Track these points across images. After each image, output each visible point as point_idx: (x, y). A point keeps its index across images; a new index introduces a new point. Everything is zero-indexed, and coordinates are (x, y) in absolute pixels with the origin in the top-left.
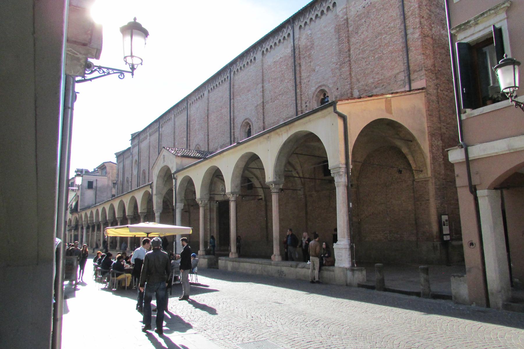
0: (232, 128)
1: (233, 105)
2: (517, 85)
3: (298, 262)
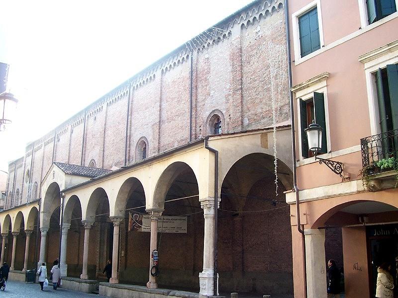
0: (128, 146)
1: (131, 121)
2: (320, 147)
3: (169, 290)
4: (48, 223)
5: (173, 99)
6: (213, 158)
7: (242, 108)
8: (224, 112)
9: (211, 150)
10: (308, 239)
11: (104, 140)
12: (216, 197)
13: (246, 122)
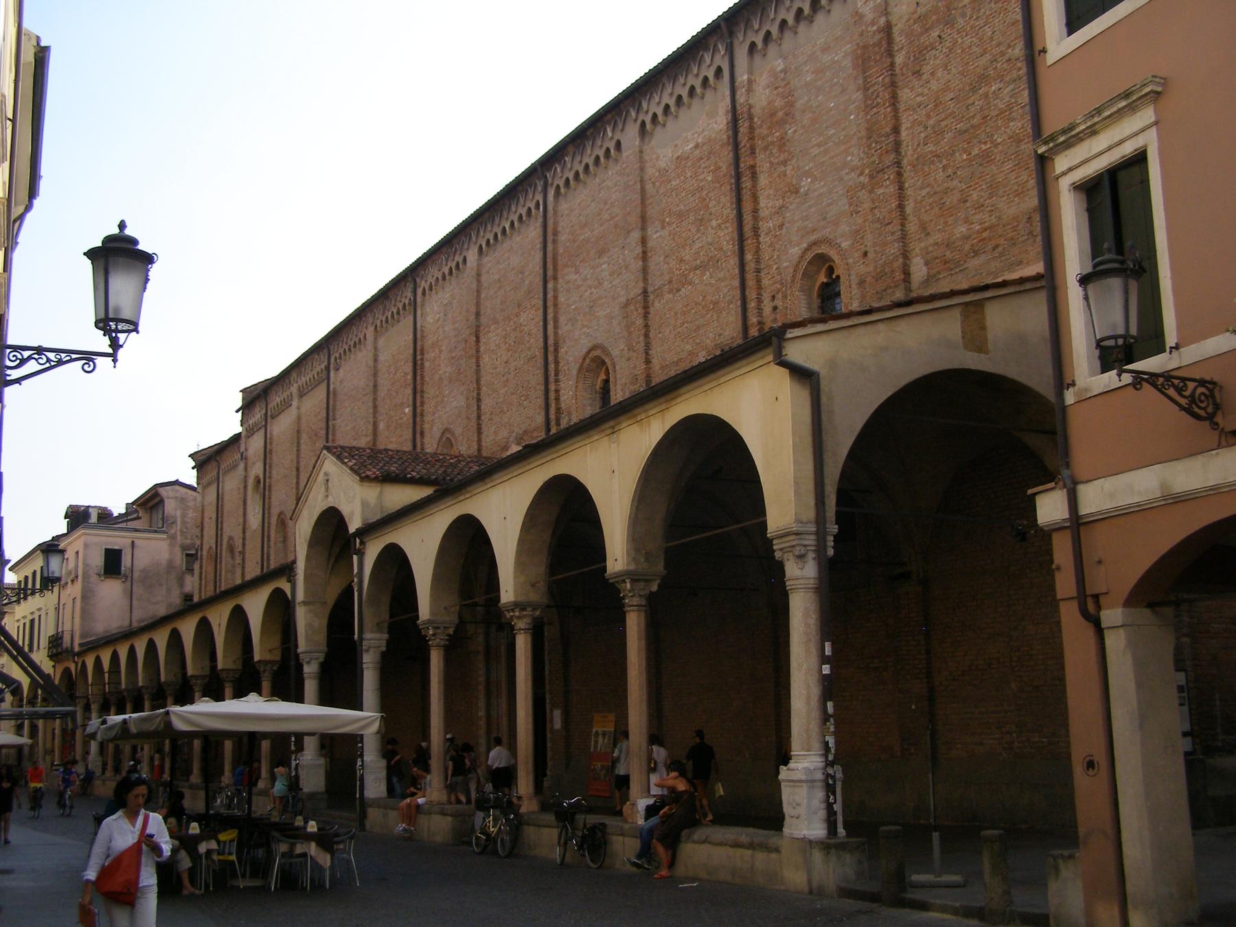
0: (552, 379)
1: (556, 298)
4: (322, 638)
5: (681, 216)
6: (804, 395)
7: (903, 225)
8: (845, 245)
9: (801, 374)
10: (1115, 643)
11: (478, 366)
12: (820, 519)
13: (919, 270)
